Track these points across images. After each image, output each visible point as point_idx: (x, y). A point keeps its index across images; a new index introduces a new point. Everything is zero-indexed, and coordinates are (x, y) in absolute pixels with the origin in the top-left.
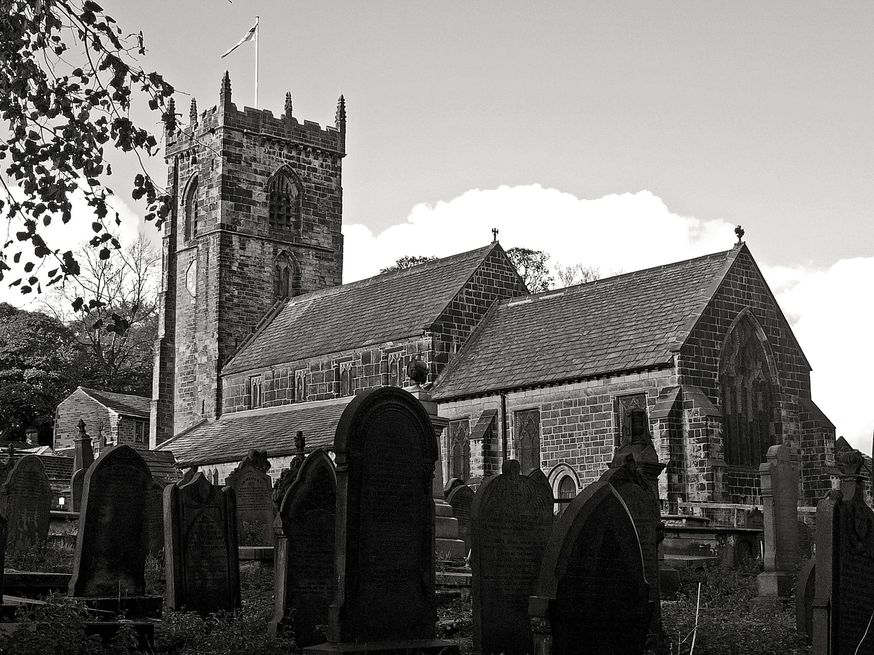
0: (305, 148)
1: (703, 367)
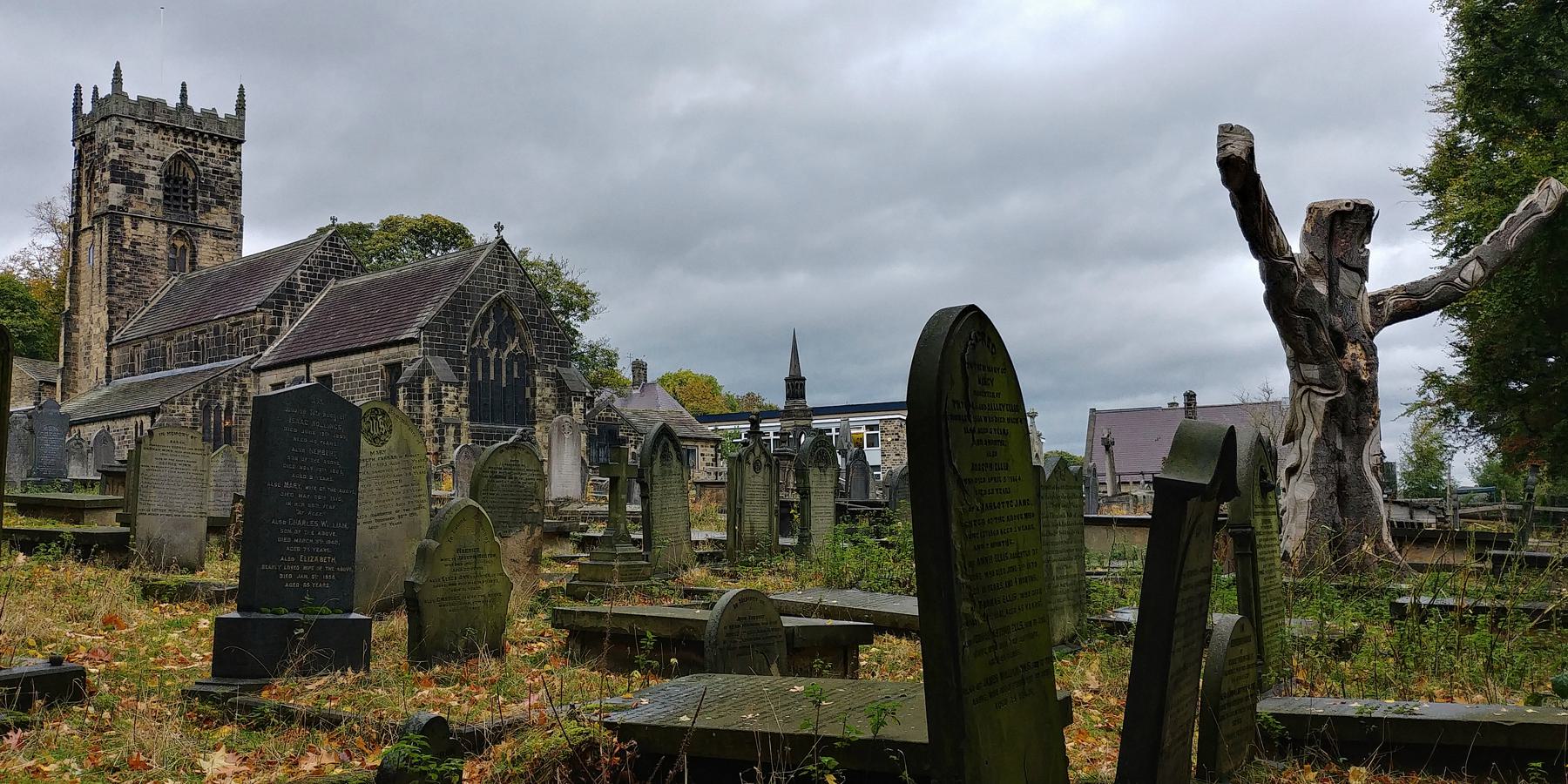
0: (202, 134)
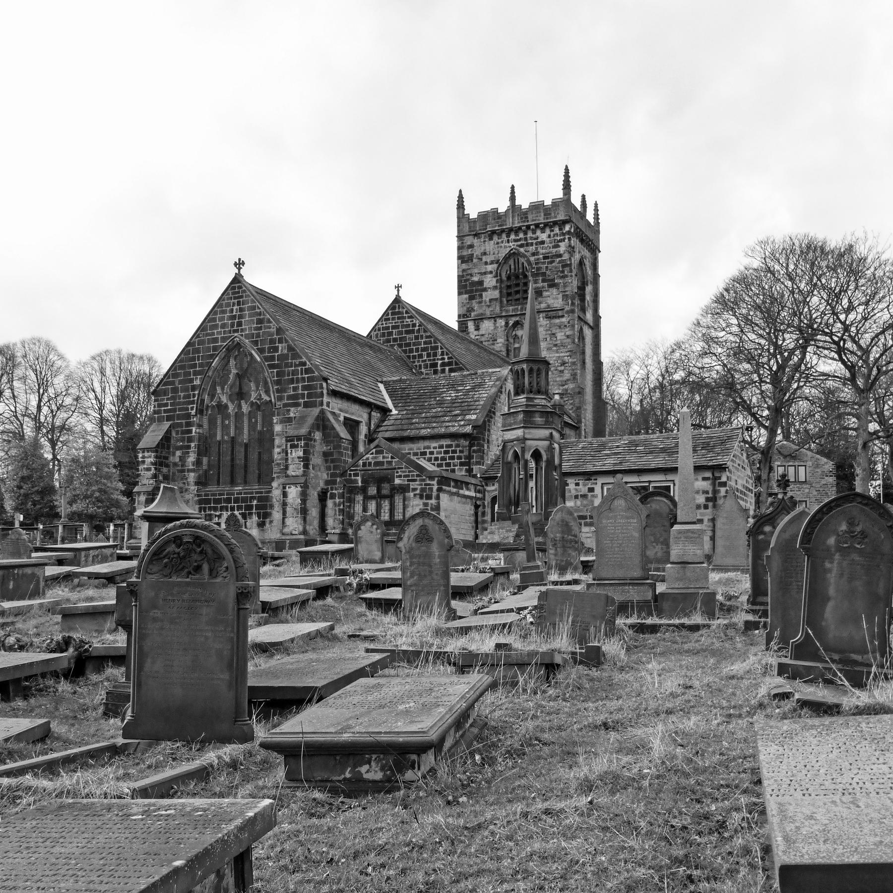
0: (528, 227)
1: (179, 404)
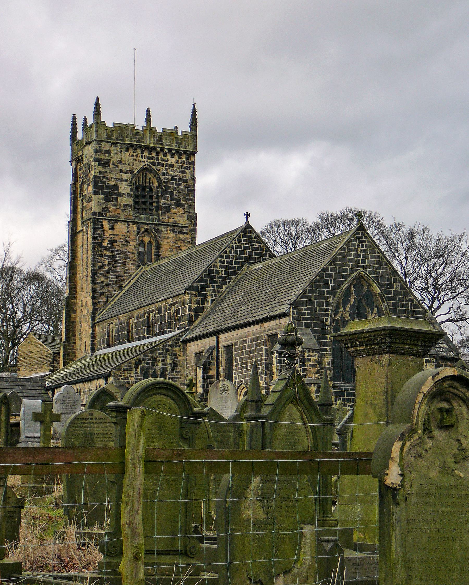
0: (162, 150)
1: (315, 315)
